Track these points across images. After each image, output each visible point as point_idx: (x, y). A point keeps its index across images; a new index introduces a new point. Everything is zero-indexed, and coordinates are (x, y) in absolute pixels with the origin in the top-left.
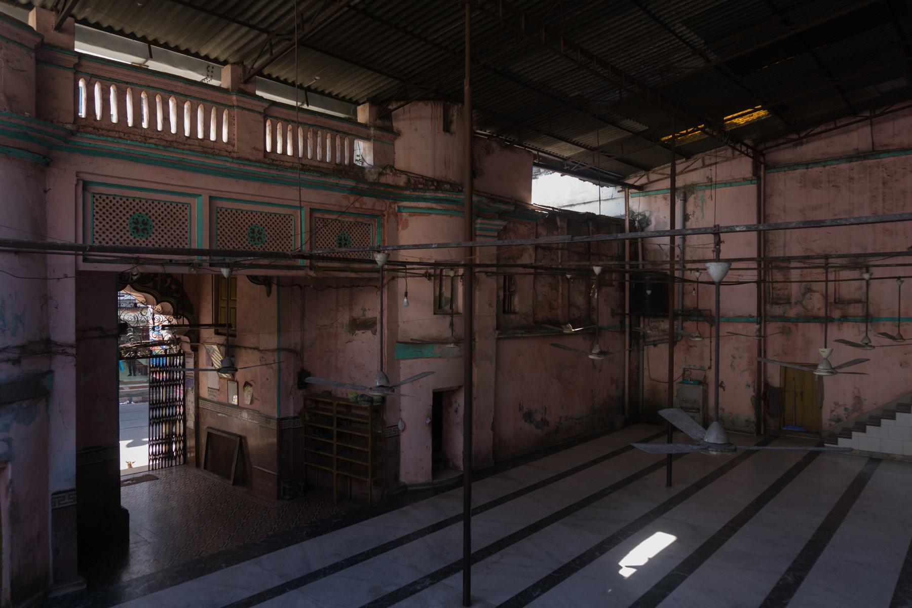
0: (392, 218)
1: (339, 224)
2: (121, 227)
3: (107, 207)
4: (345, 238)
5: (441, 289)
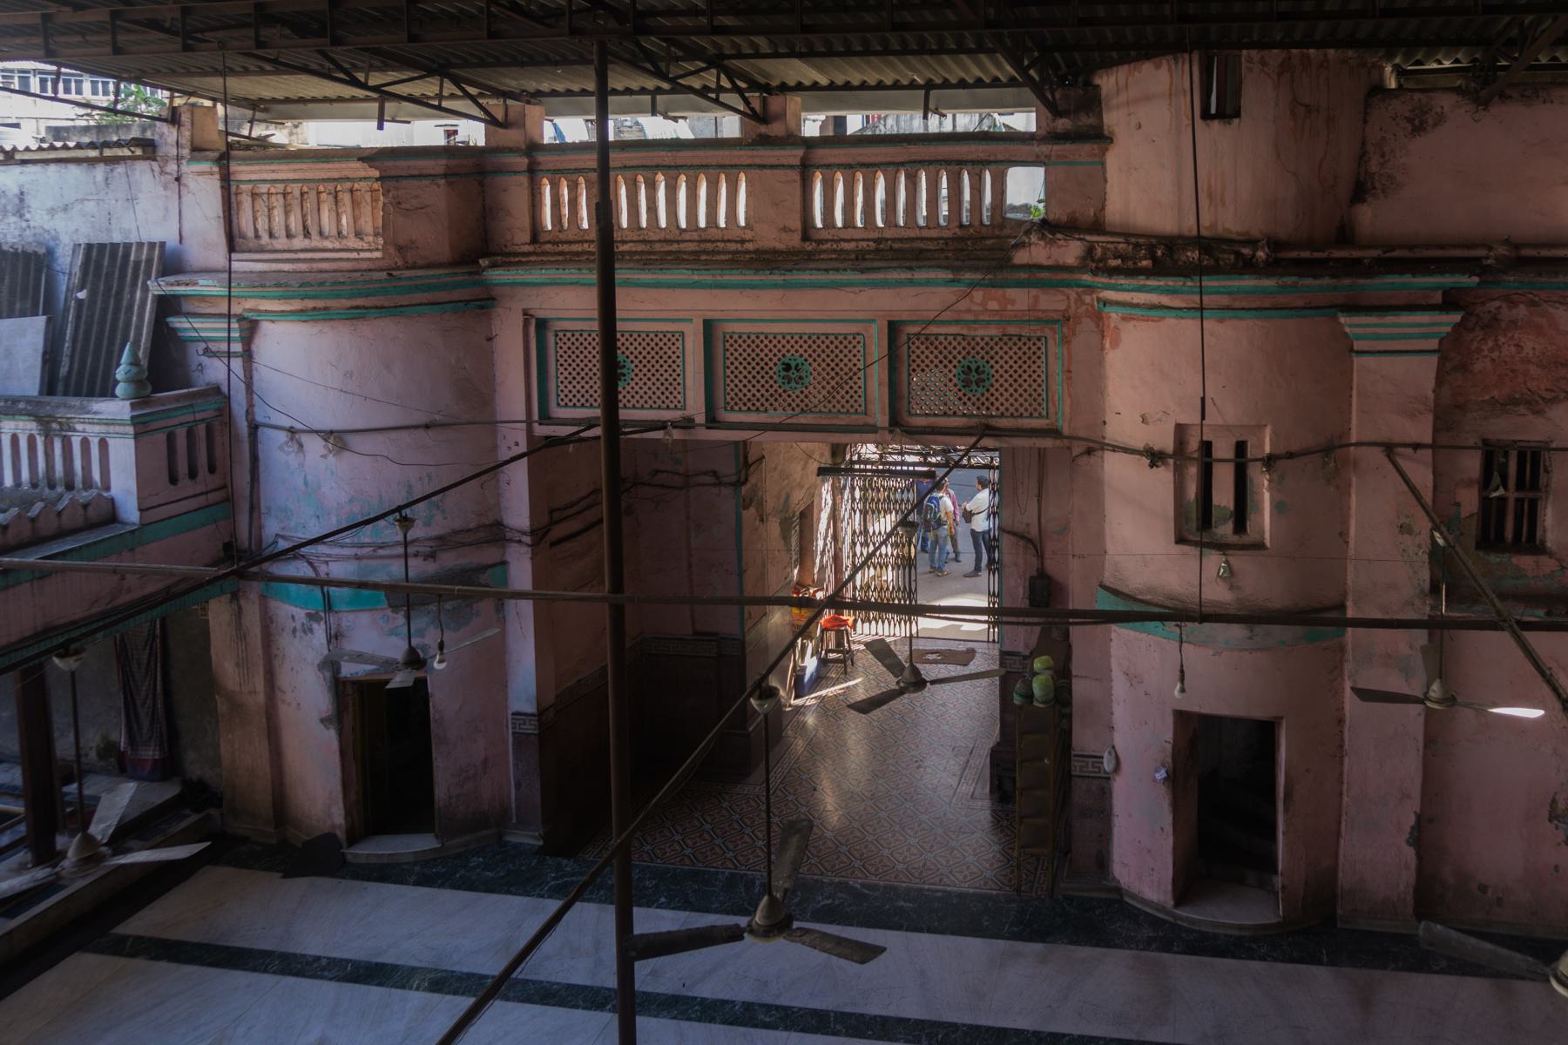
0: (1088, 324)
1: (964, 344)
3: (573, 348)
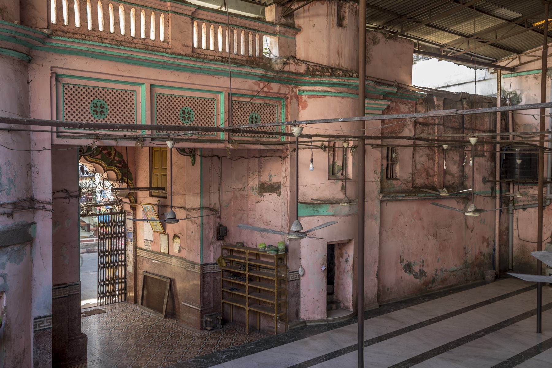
0: (294, 100)
1: (251, 106)
2: (84, 110)
3: (74, 95)
4: (256, 117)
5: (334, 159)
